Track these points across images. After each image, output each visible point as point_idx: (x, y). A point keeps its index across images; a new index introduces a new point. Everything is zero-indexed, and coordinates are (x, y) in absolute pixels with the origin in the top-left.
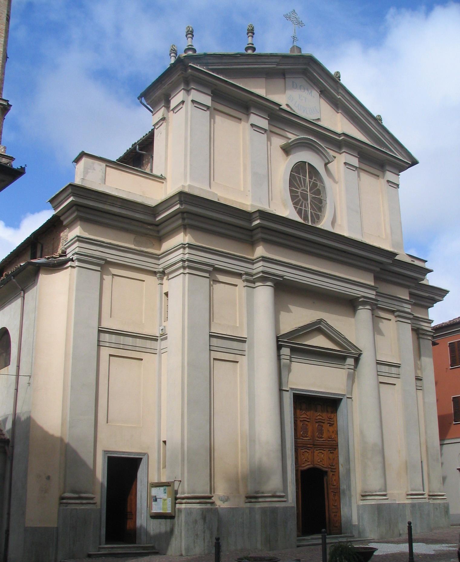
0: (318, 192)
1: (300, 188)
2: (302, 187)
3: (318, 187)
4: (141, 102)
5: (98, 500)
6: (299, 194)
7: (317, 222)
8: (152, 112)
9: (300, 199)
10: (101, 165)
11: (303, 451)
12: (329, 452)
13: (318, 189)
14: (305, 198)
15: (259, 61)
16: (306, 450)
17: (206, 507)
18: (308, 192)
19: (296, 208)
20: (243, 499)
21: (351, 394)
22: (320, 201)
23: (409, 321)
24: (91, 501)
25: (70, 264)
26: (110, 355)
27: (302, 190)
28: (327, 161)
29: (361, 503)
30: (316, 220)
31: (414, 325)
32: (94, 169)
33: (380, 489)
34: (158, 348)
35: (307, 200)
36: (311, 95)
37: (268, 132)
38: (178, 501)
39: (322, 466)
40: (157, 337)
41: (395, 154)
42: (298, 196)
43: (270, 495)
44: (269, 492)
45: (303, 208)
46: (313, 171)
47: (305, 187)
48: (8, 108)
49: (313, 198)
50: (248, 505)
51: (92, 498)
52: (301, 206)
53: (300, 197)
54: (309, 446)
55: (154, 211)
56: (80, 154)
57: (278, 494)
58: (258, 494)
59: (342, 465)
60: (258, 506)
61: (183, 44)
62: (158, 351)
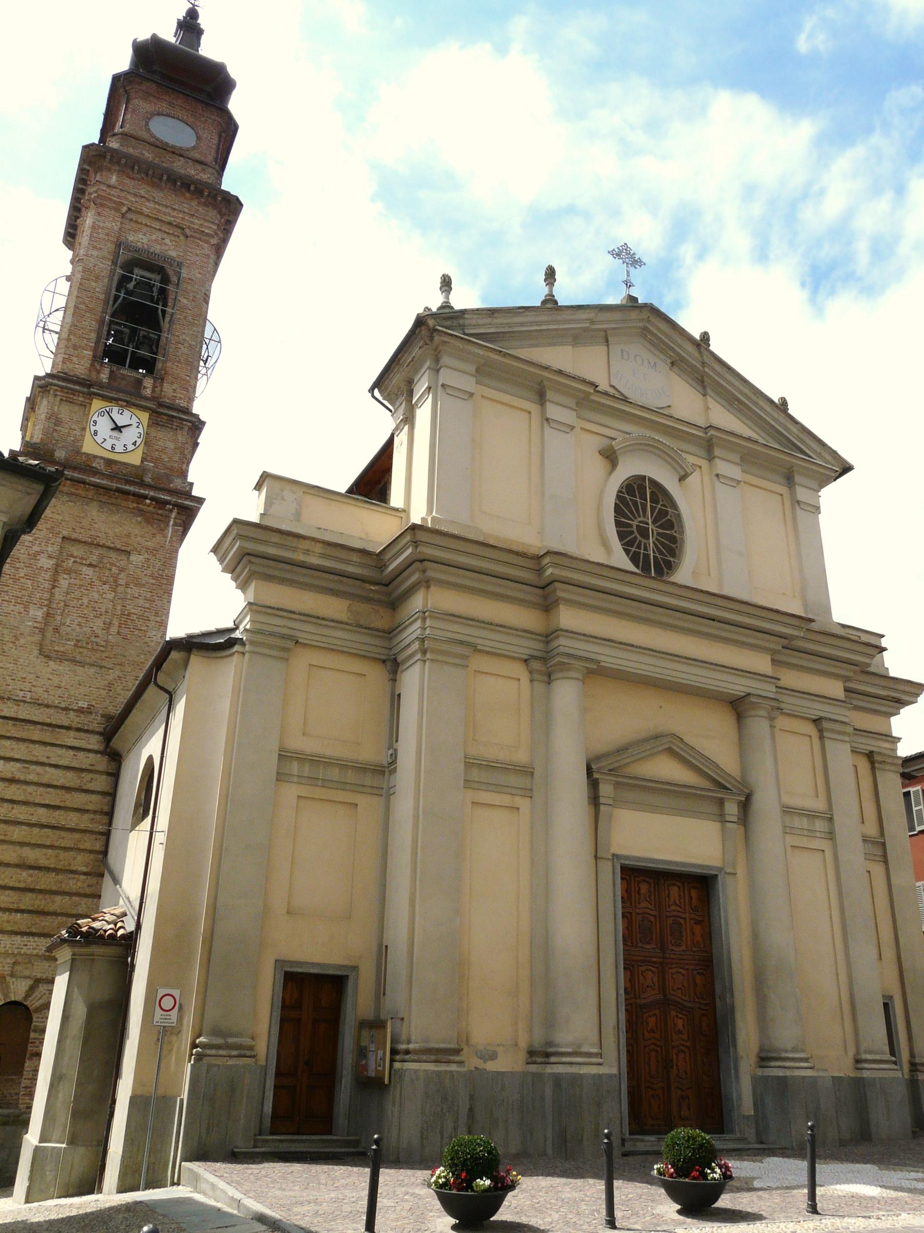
0: (670, 525)
1: (636, 518)
2: (640, 516)
3: (669, 517)
4: (373, 397)
5: (261, 1047)
6: (635, 527)
7: (668, 573)
8: (390, 411)
9: (636, 536)
10: (294, 493)
11: (643, 969)
12: (695, 972)
13: (668, 520)
14: (644, 533)
15: (559, 318)
16: (649, 968)
17: (437, 1069)
18: (648, 524)
19: (627, 552)
20: (522, 1056)
21: (734, 868)
22: (673, 540)
23: (847, 739)
24: (248, 1053)
25: (237, 648)
26: (299, 797)
27: (640, 522)
28: (683, 473)
29: (759, 1072)
30: (665, 570)
31: (854, 745)
32: (283, 499)
33: (793, 1048)
34: (385, 786)
35: (648, 538)
36: (656, 371)
37: (577, 429)
38: (398, 1057)
39: (682, 999)
40: (385, 767)
41: (810, 457)
42: (632, 532)
43: (570, 1050)
44: (567, 1046)
45: (642, 551)
46: (659, 492)
47: (644, 516)
48: (200, 426)
49: (658, 534)
50: (533, 1068)
51: (251, 1048)
52: (639, 547)
53: (636, 534)
54: (653, 959)
55: (377, 559)
56: (261, 477)
57: (585, 1049)
58: (550, 1047)
59: (720, 997)
60: (550, 1069)
61: (435, 302)
62: (384, 791)
